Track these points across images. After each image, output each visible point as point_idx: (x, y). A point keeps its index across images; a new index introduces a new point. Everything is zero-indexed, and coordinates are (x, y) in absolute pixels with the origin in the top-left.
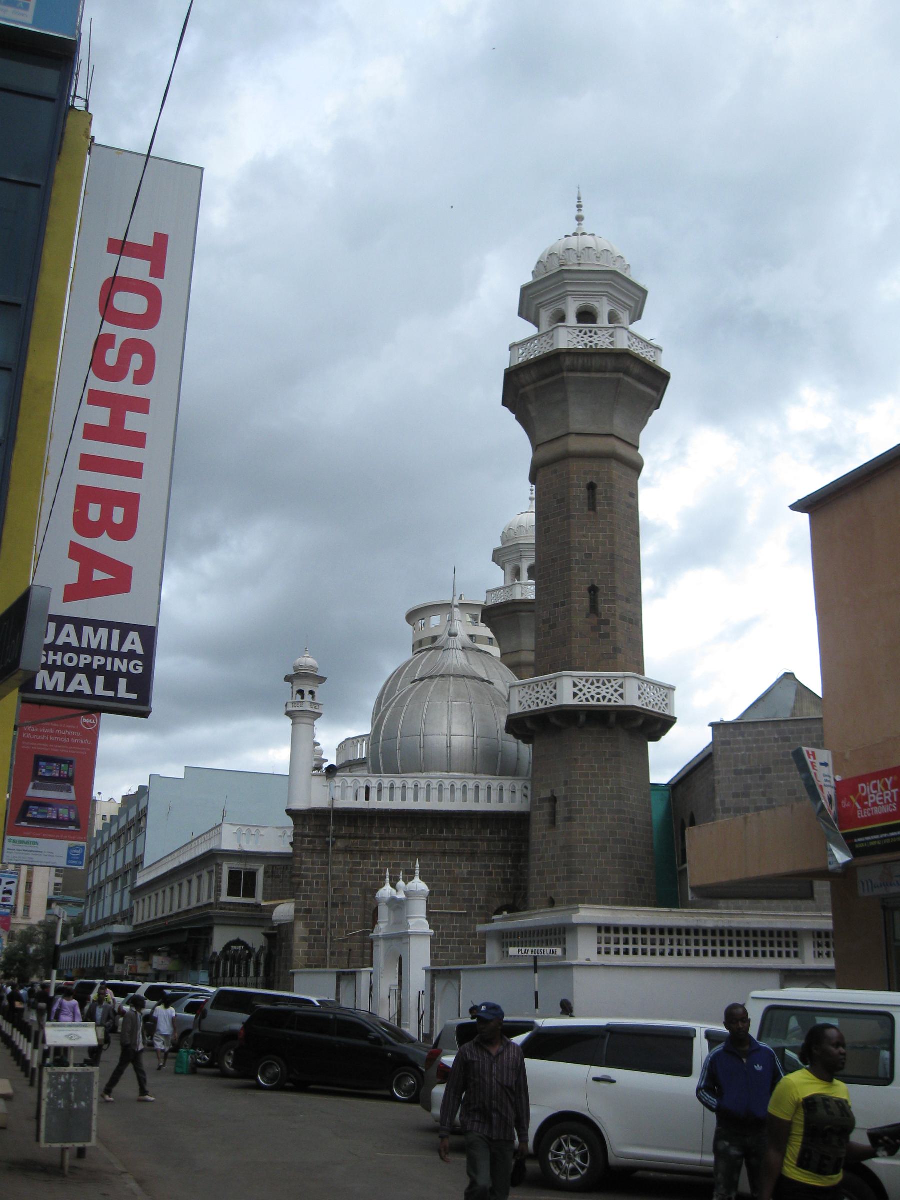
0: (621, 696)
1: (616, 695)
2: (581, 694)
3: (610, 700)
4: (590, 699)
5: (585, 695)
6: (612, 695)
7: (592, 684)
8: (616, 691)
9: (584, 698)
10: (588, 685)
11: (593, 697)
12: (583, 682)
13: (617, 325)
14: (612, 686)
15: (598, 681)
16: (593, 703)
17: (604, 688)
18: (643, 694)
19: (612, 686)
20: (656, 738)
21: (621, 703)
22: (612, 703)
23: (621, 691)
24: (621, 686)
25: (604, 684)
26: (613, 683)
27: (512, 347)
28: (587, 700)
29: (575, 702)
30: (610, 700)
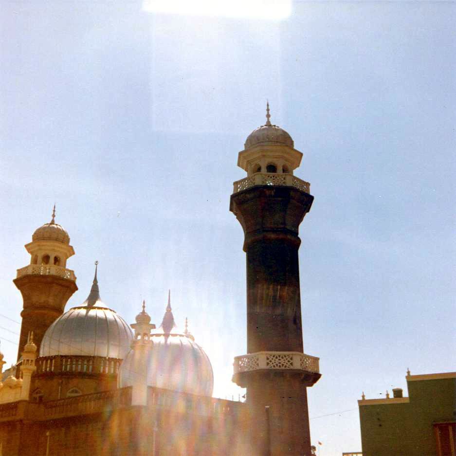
0: (291, 364)
1: (270, 359)
2: (289, 359)
3: (286, 367)
4: (276, 366)
5: (273, 363)
6: (287, 364)
7: (277, 358)
8: (271, 361)
9: (272, 365)
10: (274, 358)
11: (277, 365)
12: (272, 357)
13: (287, 174)
14: (287, 359)
15: (274, 176)
16: (277, 368)
17: (277, 363)
18: (303, 363)
19: (287, 359)
20: (311, 385)
21: (292, 367)
22: (287, 368)
23: (268, 361)
24: (291, 359)
25: (282, 358)
26: (287, 357)
27: (236, 184)
28: (274, 366)
29: (268, 367)
30: (286, 367)
